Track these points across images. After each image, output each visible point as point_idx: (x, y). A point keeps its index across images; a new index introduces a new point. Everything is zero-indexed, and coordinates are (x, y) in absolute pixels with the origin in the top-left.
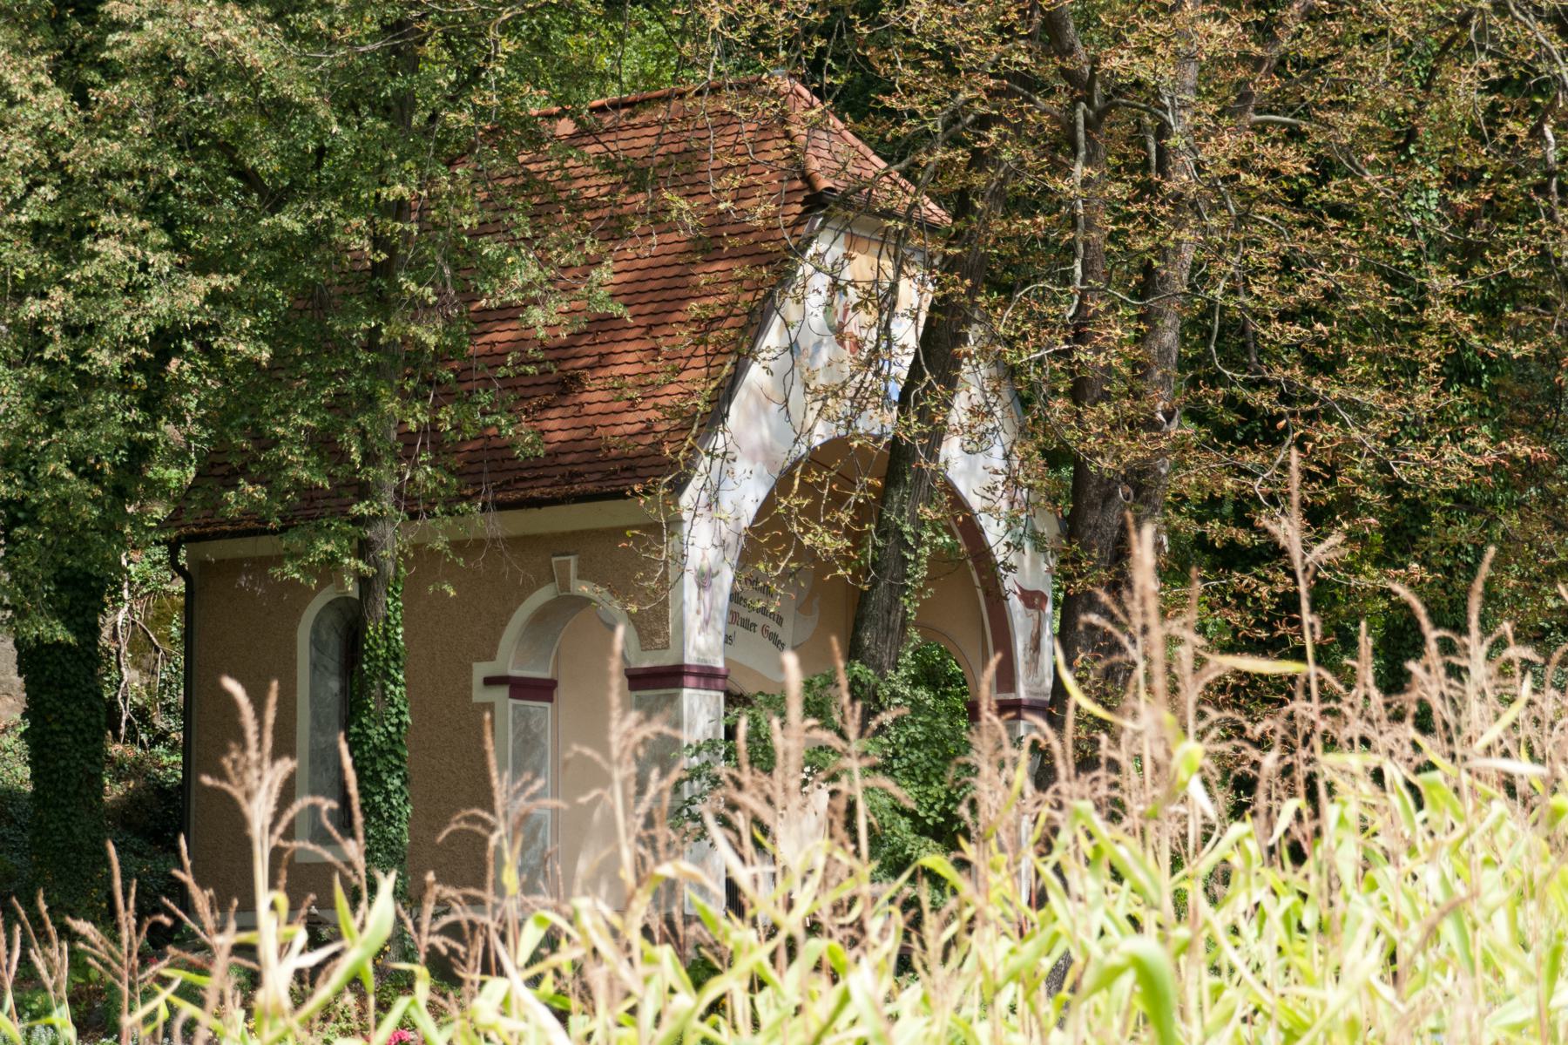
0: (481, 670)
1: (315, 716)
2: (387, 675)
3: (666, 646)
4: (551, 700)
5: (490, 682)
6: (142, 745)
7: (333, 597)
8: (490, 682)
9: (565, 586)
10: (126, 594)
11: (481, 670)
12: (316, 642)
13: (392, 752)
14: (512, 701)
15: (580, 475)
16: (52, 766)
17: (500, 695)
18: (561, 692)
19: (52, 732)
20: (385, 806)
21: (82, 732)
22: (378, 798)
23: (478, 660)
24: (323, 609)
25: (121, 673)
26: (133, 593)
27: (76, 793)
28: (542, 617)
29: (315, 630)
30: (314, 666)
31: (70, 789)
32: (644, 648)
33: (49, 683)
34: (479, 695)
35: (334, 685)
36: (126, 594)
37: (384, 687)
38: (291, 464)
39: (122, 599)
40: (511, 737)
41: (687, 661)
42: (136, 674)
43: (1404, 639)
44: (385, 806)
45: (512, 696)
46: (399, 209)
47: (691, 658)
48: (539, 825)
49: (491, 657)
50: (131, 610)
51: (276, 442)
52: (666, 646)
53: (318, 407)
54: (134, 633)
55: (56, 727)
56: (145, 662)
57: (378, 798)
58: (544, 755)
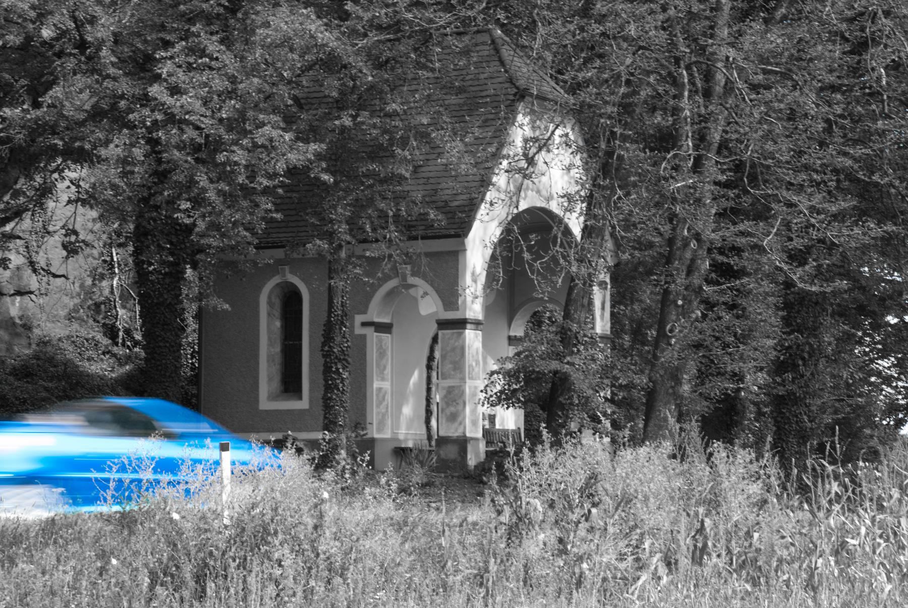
0: (359, 319)
1: (270, 339)
2: (342, 323)
3: (457, 309)
4: (390, 333)
5: (364, 324)
6: (128, 347)
7: (279, 281)
8: (364, 324)
9: (404, 278)
10: (117, 270)
11: (359, 319)
12: (270, 303)
13: (344, 359)
14: (375, 334)
15: (414, 226)
16: (158, 363)
17: (369, 332)
18: (395, 330)
19: (160, 347)
20: (341, 385)
21: (173, 346)
22: (338, 381)
23: (358, 314)
24: (274, 287)
25: (117, 312)
26: (121, 270)
27: (170, 376)
28: (391, 294)
29: (269, 297)
30: (269, 314)
31: (168, 374)
32: (446, 310)
33: (158, 323)
34: (359, 330)
35: (278, 323)
36: (117, 270)
37: (341, 329)
38: (340, 232)
39: (114, 273)
40: (375, 350)
41: (467, 317)
42: (124, 311)
43: (793, 308)
44: (341, 385)
45: (376, 331)
46: (394, 114)
47: (469, 315)
48: (386, 393)
49: (365, 312)
50: (120, 278)
51: (331, 221)
52: (457, 309)
53: (347, 205)
54: (122, 290)
55: (161, 344)
56: (128, 305)
57: (338, 381)
58: (387, 360)
